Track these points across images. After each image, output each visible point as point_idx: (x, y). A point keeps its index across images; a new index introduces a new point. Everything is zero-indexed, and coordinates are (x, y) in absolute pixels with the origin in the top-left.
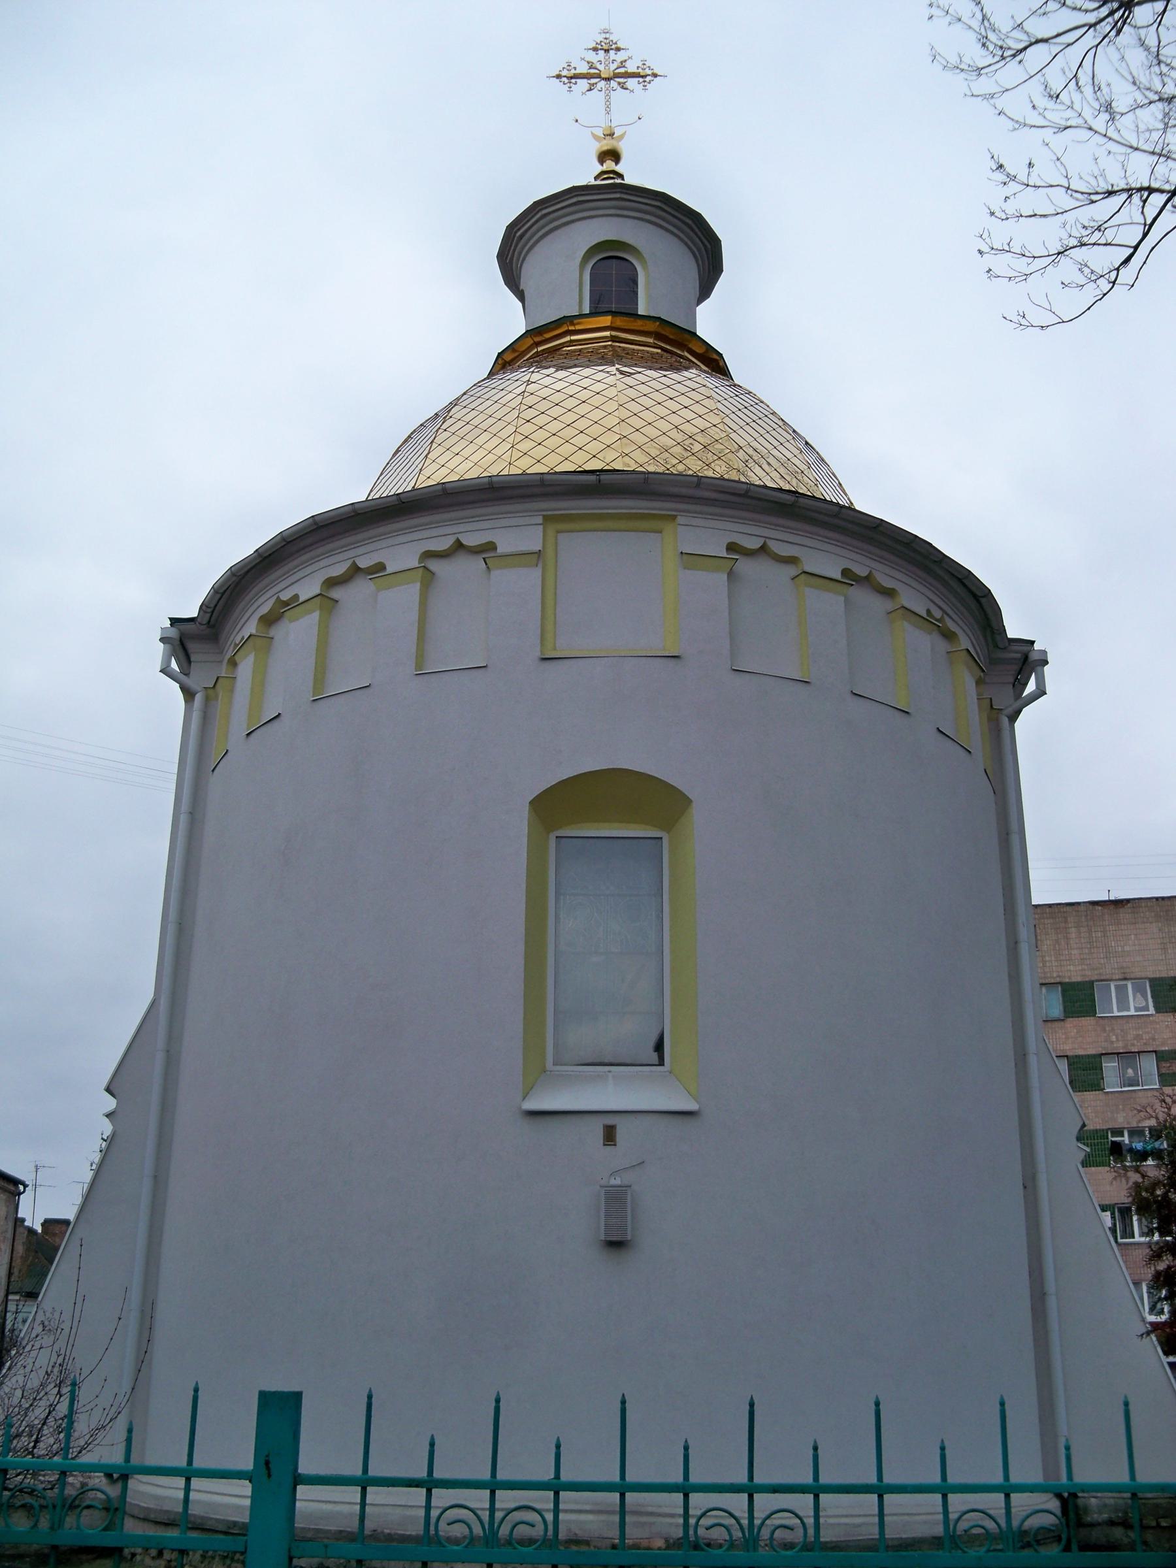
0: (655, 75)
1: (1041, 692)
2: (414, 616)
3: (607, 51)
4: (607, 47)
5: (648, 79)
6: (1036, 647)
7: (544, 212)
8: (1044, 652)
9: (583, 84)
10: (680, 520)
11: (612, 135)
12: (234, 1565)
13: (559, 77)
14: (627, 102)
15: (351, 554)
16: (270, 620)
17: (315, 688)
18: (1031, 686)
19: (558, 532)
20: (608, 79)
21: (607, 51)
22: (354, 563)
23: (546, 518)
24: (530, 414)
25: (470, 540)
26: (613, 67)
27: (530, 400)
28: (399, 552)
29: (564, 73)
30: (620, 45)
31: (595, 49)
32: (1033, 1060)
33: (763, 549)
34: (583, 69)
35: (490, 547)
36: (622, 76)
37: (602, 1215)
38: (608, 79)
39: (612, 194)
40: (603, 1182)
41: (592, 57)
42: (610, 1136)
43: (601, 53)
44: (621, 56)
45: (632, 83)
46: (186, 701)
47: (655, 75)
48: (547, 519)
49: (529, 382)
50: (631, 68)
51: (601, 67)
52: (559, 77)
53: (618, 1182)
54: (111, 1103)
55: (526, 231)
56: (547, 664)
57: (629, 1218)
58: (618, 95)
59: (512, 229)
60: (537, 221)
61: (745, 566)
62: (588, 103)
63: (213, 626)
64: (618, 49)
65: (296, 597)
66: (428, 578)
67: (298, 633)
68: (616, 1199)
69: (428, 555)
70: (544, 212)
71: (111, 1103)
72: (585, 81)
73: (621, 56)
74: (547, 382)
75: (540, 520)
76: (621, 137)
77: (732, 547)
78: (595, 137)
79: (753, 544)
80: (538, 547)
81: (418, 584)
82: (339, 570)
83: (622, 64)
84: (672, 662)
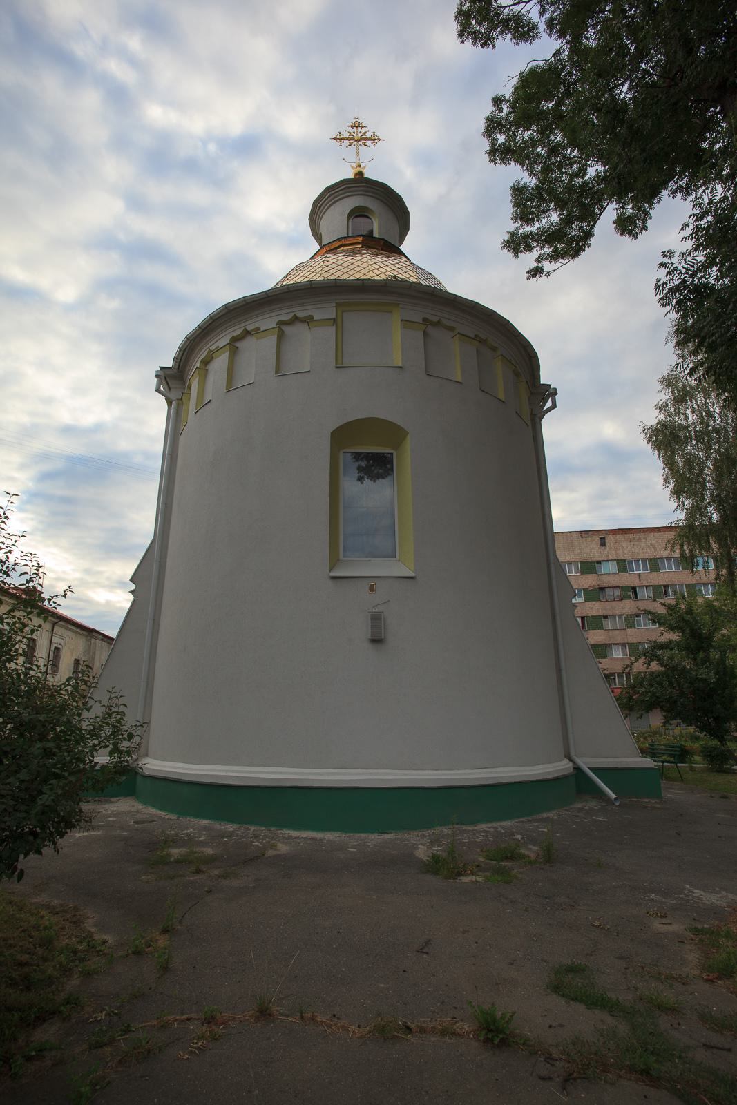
0: (380, 140)
1: (554, 406)
2: (274, 350)
3: (357, 127)
4: (358, 126)
5: (376, 141)
6: (552, 387)
7: (331, 193)
8: (556, 389)
9: (346, 142)
10: (401, 306)
11: (360, 166)
12: (2, 907)
13: (335, 139)
14: (367, 151)
15: (244, 324)
16: (206, 362)
17: (227, 386)
18: (549, 404)
19: (343, 312)
20: (358, 140)
21: (357, 127)
22: (245, 329)
23: (337, 303)
24: (326, 269)
25: (301, 315)
26: (360, 135)
27: (327, 264)
28: (267, 322)
29: (338, 137)
30: (363, 125)
31: (351, 126)
32: (552, 565)
33: (439, 322)
34: (346, 135)
35: (311, 317)
36: (363, 139)
37: (370, 626)
38: (358, 140)
39: (360, 184)
40: (370, 610)
41: (350, 130)
42: (372, 589)
43: (355, 128)
44: (364, 130)
45: (369, 143)
46: (168, 405)
47: (380, 140)
48: (338, 305)
49: (326, 257)
50: (368, 135)
51: (355, 135)
52: (335, 139)
53: (376, 610)
54: (133, 587)
55: (323, 203)
56: (339, 370)
57: (383, 628)
58: (363, 148)
59: (316, 202)
60: (327, 198)
61: (431, 330)
62: (348, 151)
63: (181, 372)
64: (363, 127)
65: (218, 347)
66: (281, 336)
67: (220, 365)
68: (376, 619)
69: (281, 323)
70: (331, 193)
71: (133, 587)
72: (347, 141)
73: (364, 130)
74: (332, 258)
75: (334, 304)
76: (365, 167)
77: (425, 320)
78: (352, 167)
79: (435, 319)
80: (334, 316)
81: (276, 336)
82: (238, 333)
83: (364, 134)
84: (398, 370)
